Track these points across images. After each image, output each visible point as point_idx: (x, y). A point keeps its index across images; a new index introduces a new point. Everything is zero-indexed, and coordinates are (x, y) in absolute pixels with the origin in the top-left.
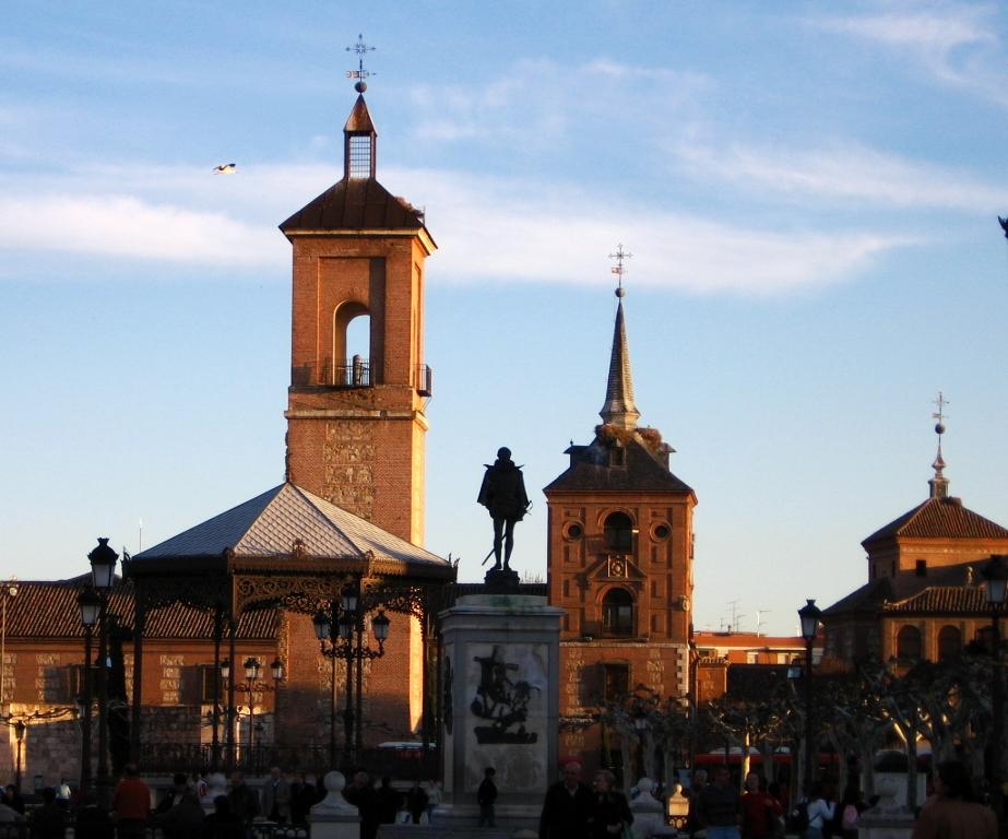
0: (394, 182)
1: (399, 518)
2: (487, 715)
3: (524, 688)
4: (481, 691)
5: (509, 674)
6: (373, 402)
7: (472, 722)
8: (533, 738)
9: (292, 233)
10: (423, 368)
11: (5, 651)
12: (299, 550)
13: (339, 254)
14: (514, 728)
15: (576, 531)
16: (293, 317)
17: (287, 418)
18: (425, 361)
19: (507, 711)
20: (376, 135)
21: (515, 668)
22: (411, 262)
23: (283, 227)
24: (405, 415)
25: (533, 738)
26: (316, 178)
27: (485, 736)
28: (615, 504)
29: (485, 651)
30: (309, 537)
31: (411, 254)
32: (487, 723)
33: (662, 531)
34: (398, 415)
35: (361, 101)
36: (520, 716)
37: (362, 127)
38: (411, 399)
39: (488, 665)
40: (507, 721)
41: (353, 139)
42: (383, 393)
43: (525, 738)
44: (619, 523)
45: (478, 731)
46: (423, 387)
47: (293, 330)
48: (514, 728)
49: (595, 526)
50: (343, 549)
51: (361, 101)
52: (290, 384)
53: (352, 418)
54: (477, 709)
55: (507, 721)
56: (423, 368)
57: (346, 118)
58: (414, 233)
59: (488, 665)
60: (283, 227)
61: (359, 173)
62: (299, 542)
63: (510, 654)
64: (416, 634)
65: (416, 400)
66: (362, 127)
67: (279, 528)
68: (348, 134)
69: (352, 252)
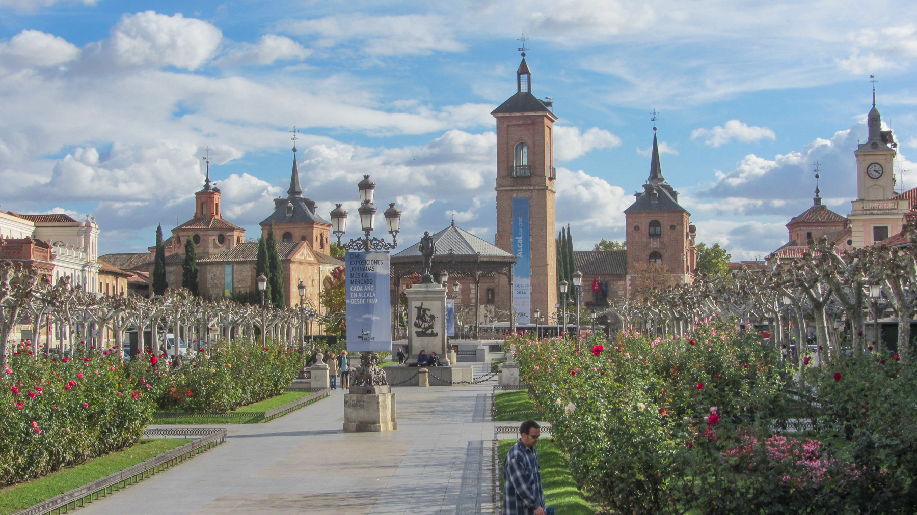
0: (539, 93)
2: (420, 327)
3: (433, 317)
4: (417, 318)
5: (427, 312)
7: (415, 329)
8: (436, 335)
14: (429, 331)
15: (637, 228)
19: (427, 325)
25: (436, 335)
26: (508, 91)
27: (419, 334)
28: (654, 217)
29: (418, 304)
32: (420, 330)
33: (673, 227)
36: (431, 327)
37: (523, 70)
39: (419, 309)
40: (427, 329)
42: (534, 180)
43: (434, 335)
44: (654, 224)
45: (417, 333)
48: (429, 331)
49: (644, 227)
50: (466, 252)
54: (416, 325)
55: (427, 329)
57: (516, 67)
59: (419, 309)
61: (524, 89)
63: (426, 305)
65: (547, 181)
66: (523, 70)
68: (519, 74)
69: (520, 122)
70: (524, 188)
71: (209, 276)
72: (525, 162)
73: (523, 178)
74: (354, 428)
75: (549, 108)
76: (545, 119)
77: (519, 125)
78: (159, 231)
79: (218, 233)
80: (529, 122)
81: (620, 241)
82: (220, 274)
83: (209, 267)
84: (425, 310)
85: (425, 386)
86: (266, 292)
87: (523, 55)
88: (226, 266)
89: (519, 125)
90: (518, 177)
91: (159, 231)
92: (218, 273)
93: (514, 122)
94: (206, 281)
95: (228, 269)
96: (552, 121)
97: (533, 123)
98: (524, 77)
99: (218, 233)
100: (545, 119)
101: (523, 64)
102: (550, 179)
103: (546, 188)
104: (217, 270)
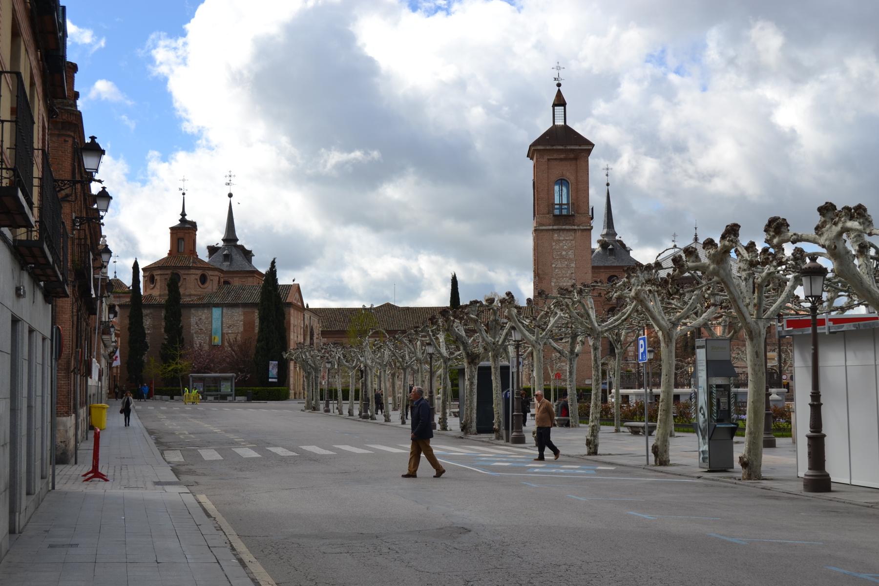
26: (543, 125)
37: (560, 101)
61: (560, 122)
66: (560, 101)
68: (554, 105)
69: (562, 156)
70: (567, 227)
71: (193, 320)
73: (327, 405)
74: (710, 383)
79: (199, 272)
80: (572, 156)
82: (207, 318)
83: (193, 311)
85: (555, 390)
87: (559, 85)
88: (214, 310)
89: (561, 160)
92: (203, 317)
93: (555, 156)
94: (190, 326)
95: (216, 312)
97: (576, 159)
98: (559, 110)
99: (199, 272)
101: (559, 94)
104: (203, 314)
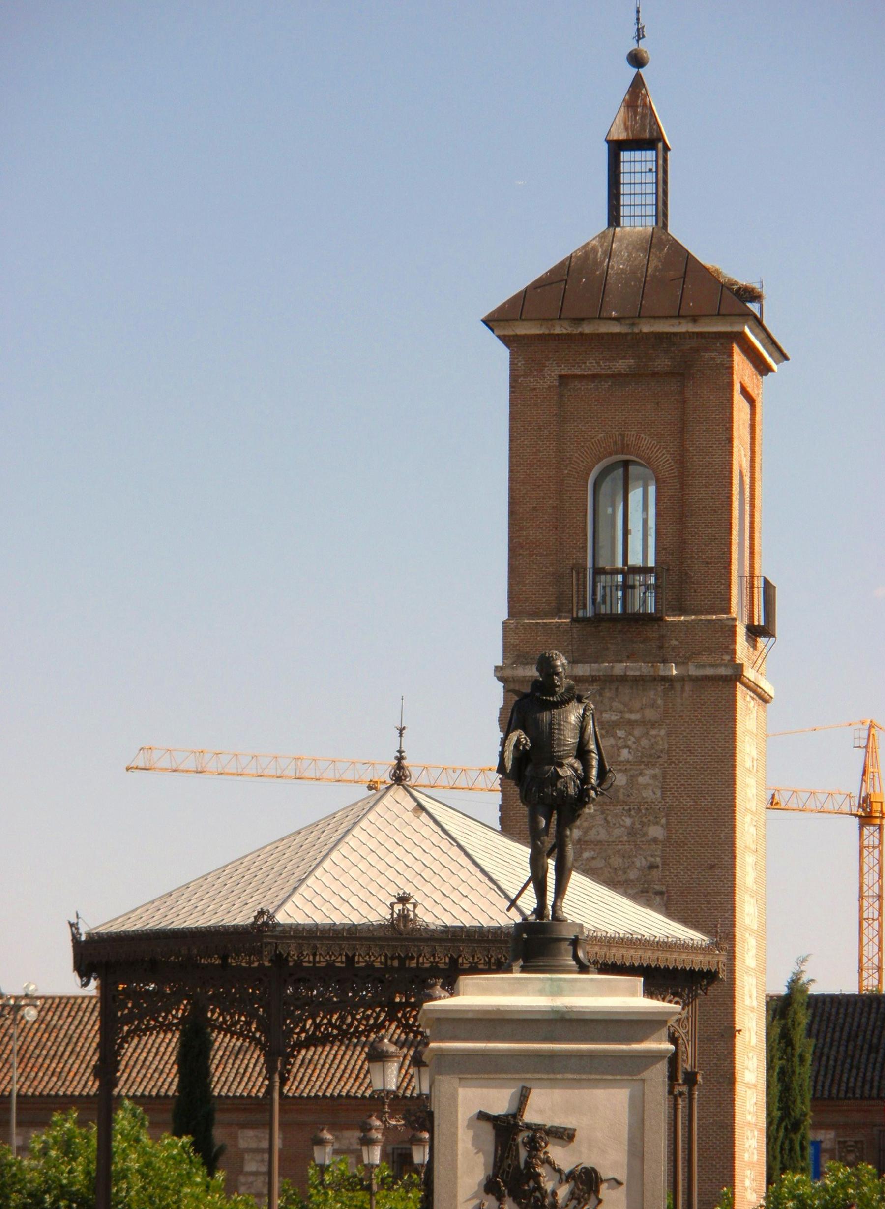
1: (712, 867)
6: (661, 647)
9: (509, 332)
10: (759, 583)
11: (19, 1124)
12: (404, 917)
13: (595, 371)
16: (511, 490)
17: (500, 679)
18: (762, 569)
20: (666, 148)
21: (565, 1135)
22: (731, 384)
23: (490, 322)
24: (723, 671)
29: (499, 1101)
30: (427, 889)
31: (731, 368)
34: (709, 671)
35: (638, 84)
37: (640, 135)
38: (734, 642)
39: (505, 1130)
41: (625, 156)
46: (759, 620)
47: (512, 513)
51: (638, 84)
52: (505, 616)
53: (623, 679)
56: (759, 583)
57: (609, 118)
58: (736, 329)
59: (505, 1130)
60: (490, 322)
62: (403, 899)
63: (544, 1107)
64: (749, 1086)
66: (640, 135)
67: (372, 873)
68: (616, 148)
69: (622, 365)
72: (641, 550)
75: (754, 307)
76: (739, 358)
77: (617, 378)
78: (763, 698)
80: (663, 363)
81: (315, 1148)
84: (540, 1136)
86: (27, 1022)
90: (601, 621)
91: (763, 698)
93: (591, 365)
96: (763, 368)
97: (682, 373)
100: (739, 358)
102: (755, 632)
103: (736, 675)
